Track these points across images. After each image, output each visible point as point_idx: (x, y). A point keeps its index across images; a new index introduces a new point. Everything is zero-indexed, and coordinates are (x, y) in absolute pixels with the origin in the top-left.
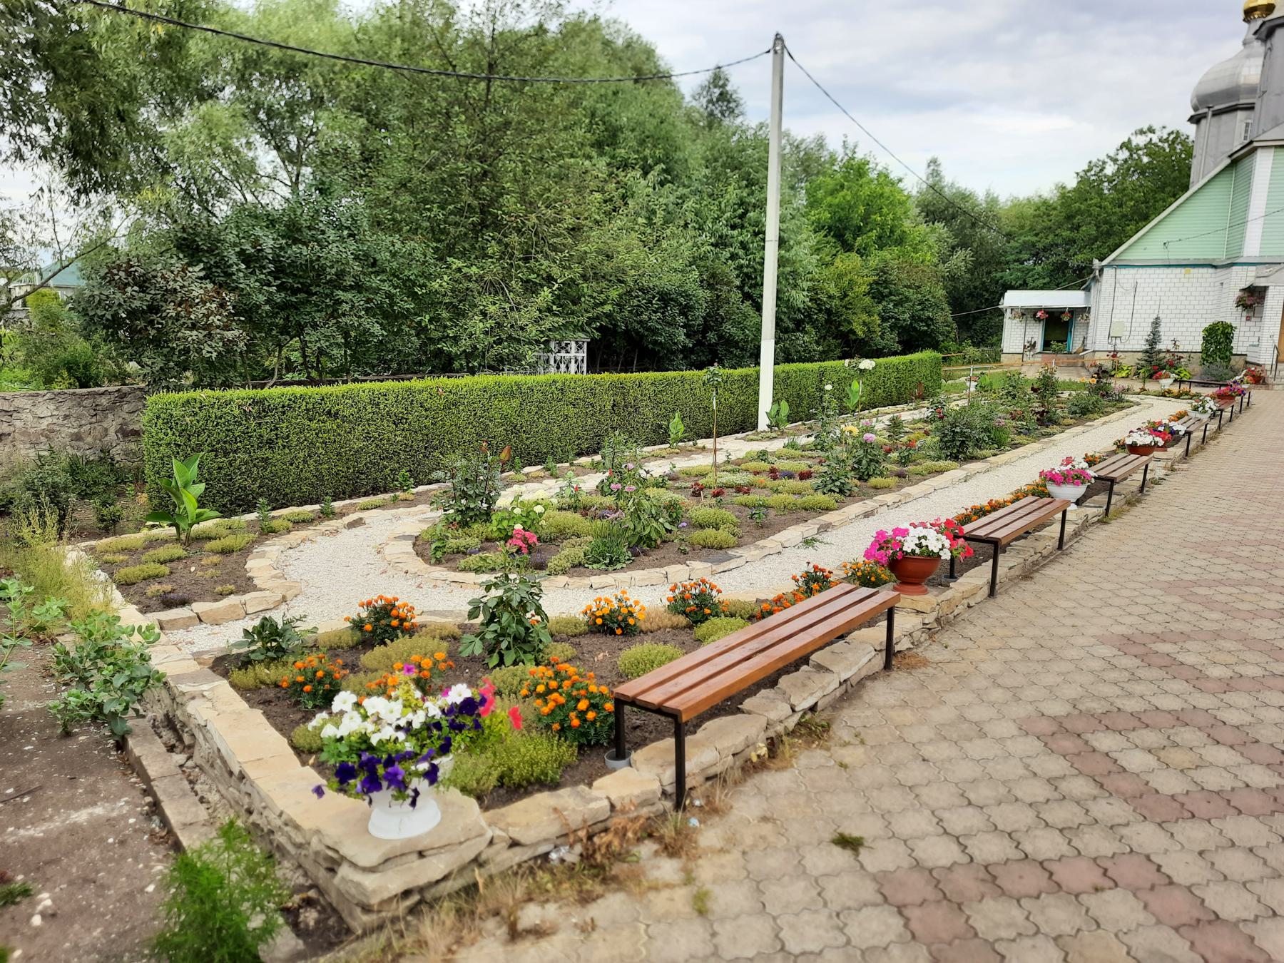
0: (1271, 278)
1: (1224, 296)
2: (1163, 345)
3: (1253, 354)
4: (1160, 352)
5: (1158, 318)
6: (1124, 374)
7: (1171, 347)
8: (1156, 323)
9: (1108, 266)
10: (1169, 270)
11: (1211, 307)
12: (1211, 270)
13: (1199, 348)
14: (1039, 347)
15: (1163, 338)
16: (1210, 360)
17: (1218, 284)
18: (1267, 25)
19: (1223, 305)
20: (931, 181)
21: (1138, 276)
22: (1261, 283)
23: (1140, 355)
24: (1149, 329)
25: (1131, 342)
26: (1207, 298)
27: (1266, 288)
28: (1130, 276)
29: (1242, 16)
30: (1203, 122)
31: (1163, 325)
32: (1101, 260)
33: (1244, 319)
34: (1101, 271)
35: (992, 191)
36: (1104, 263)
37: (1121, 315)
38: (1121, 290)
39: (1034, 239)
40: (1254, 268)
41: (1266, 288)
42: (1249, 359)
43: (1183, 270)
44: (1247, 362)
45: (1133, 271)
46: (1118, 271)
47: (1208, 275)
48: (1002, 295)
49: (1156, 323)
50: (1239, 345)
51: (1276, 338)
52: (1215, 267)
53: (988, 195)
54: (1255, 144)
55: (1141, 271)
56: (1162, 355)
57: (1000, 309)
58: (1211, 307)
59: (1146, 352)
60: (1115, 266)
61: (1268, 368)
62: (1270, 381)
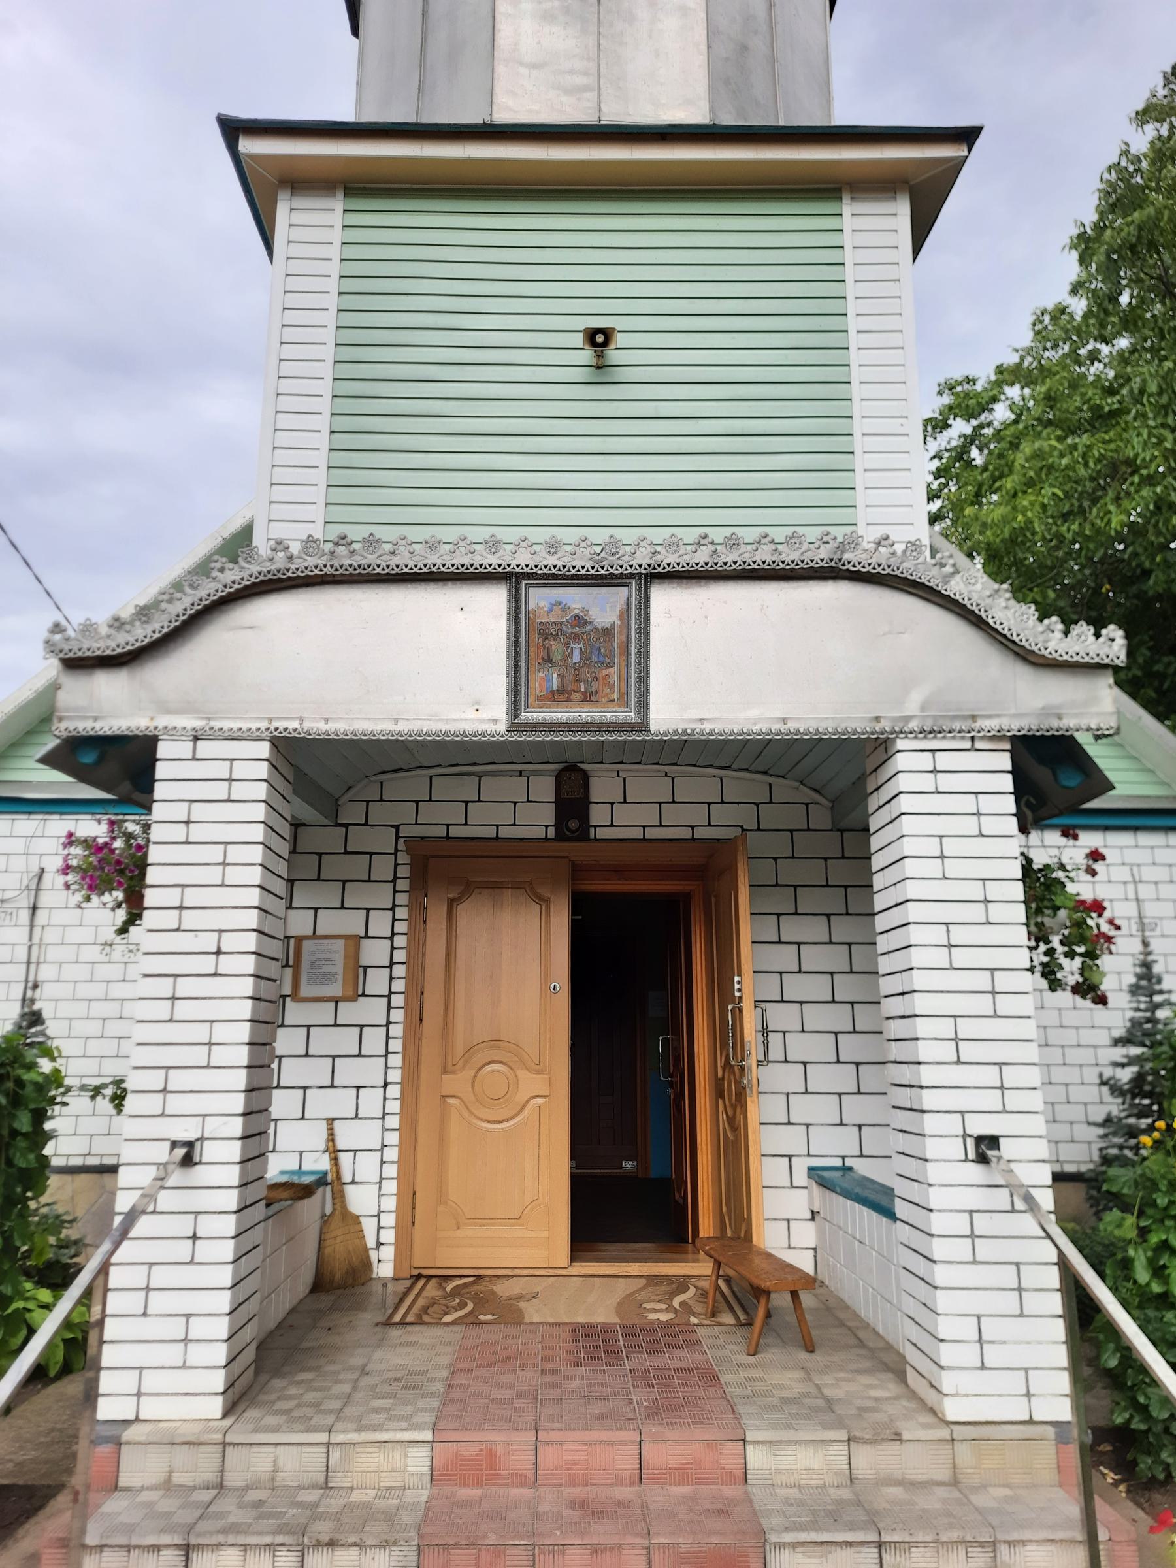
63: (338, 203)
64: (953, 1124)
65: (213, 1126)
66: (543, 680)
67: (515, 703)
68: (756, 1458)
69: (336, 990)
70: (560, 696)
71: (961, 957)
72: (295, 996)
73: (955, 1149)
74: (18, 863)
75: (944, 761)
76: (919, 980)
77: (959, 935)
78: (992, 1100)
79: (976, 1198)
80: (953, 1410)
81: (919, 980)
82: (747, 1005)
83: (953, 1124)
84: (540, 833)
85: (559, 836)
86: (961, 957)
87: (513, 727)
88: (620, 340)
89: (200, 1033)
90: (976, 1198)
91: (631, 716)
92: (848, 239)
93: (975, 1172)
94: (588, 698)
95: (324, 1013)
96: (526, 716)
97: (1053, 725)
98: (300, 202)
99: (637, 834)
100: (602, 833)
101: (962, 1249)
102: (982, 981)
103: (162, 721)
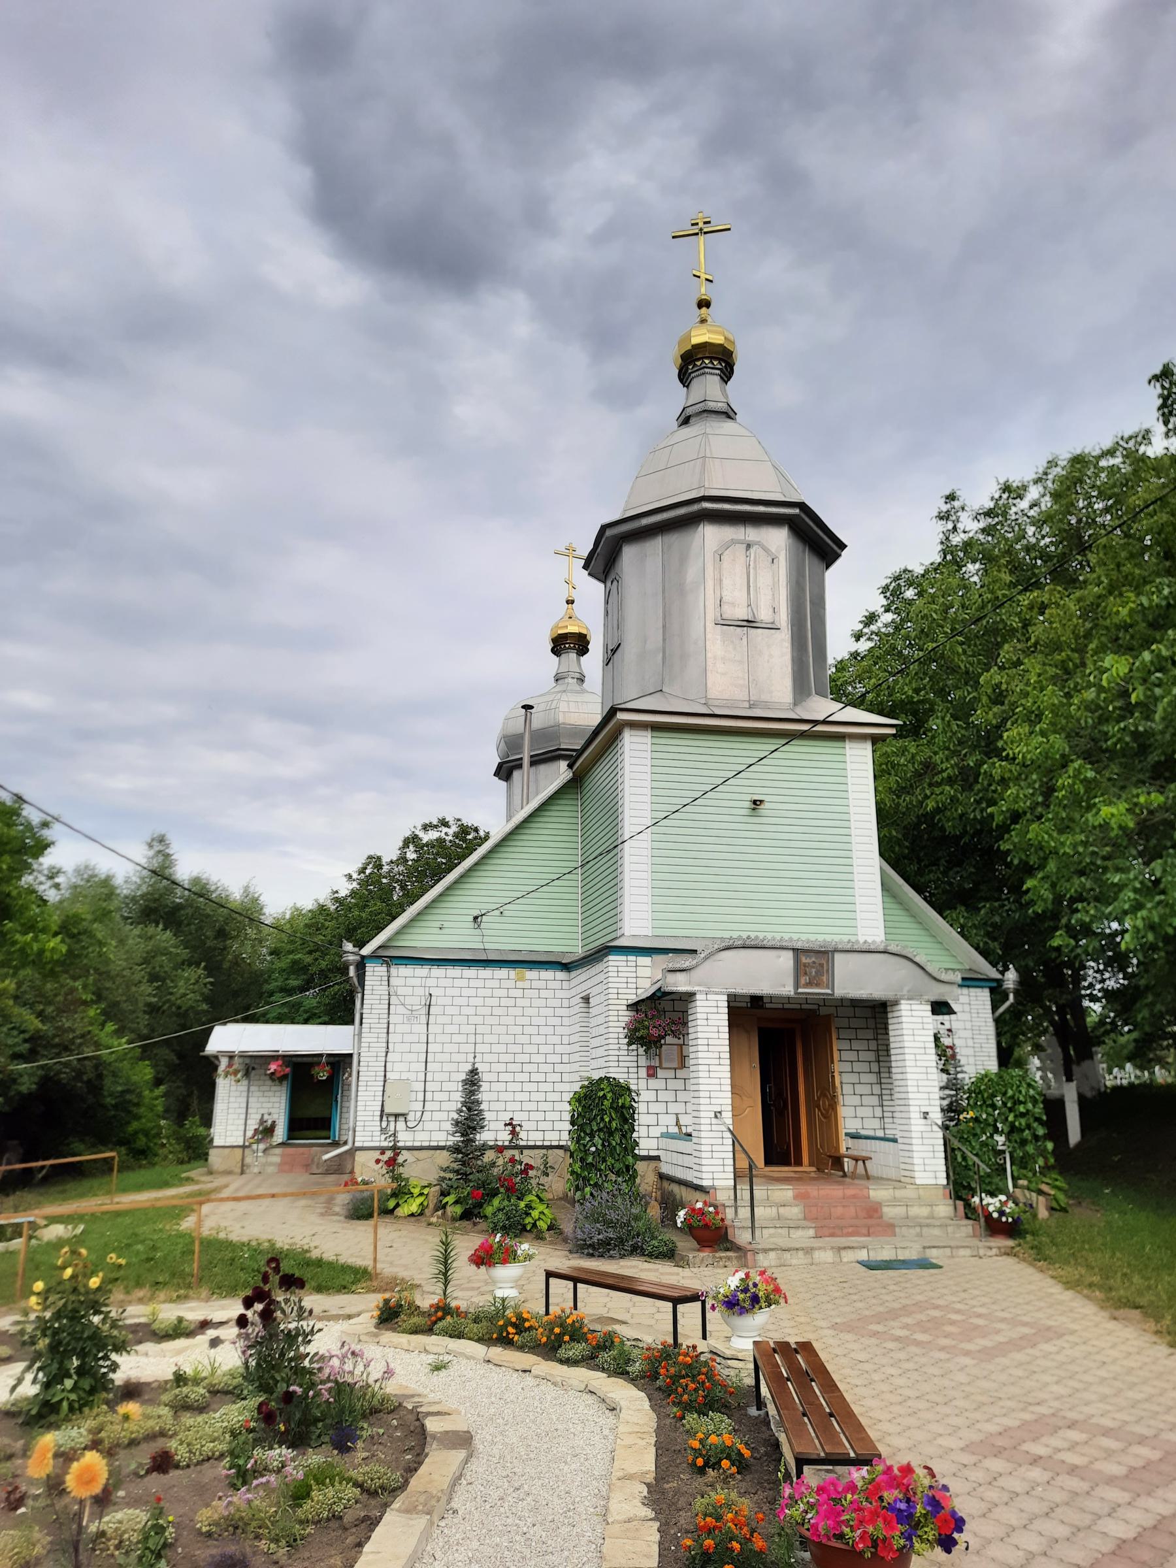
0: (695, 974)
1: (594, 1022)
2: (493, 1133)
3: (680, 1159)
4: (484, 1147)
5: (474, 1072)
6: (413, 1206)
7: (504, 1137)
8: (472, 1081)
9: (375, 956)
10: (486, 973)
11: (568, 1049)
12: (561, 975)
13: (565, 1139)
14: (280, 1134)
15: (487, 1115)
16: (594, 1177)
17: (578, 1000)
18: (609, 533)
19: (595, 1042)
20: (155, 864)
21: (431, 982)
22: (679, 984)
23: (444, 1158)
24: (458, 1097)
25: (429, 1126)
26: (559, 1030)
27: (691, 995)
28: (417, 982)
29: (550, 646)
30: (516, 774)
31: (485, 1086)
32: (361, 944)
33: (643, 1072)
34: (361, 966)
35: (251, 890)
36: (366, 951)
37: (405, 1067)
38: (401, 1010)
39: (308, 959)
40: (645, 961)
41: (691, 995)
42: (665, 1169)
43: (513, 973)
44: (662, 1177)
45: (422, 971)
46: (393, 970)
47: (557, 985)
48: (207, 1033)
49: (472, 1081)
50: (647, 1139)
51: (728, 1116)
52: (566, 967)
53: (246, 888)
54: (621, 716)
55: (437, 972)
56: (489, 1156)
57: (207, 1058)
58: (568, 1049)
59: (456, 1149)
60: (389, 958)
61: (724, 1197)
62: (742, 1237)
63: (649, 734)
64: (917, 1109)
65: (724, 1108)
66: (803, 980)
67: (797, 985)
68: (872, 1193)
69: (675, 1065)
70: (809, 984)
71: (919, 1064)
72: (661, 1068)
73: (918, 1115)
74: (420, 991)
75: (914, 1007)
76: (699, 1029)
77: (918, 1057)
78: (927, 1102)
79: (923, 1128)
80: (918, 1182)
81: (699, 1029)
82: (836, 1074)
83: (917, 1109)
84: (744, 1005)
85: (752, 1007)
86: (919, 1064)
87: (796, 993)
88: (766, 805)
89: (717, 1081)
90: (923, 1128)
91: (829, 991)
92: (848, 759)
93: (923, 1121)
94: (818, 985)
95: (671, 1074)
96: (800, 990)
97: (942, 999)
98: (634, 732)
99: (780, 1006)
100: (768, 1006)
101: (920, 1142)
102: (924, 1070)
103: (696, 988)
